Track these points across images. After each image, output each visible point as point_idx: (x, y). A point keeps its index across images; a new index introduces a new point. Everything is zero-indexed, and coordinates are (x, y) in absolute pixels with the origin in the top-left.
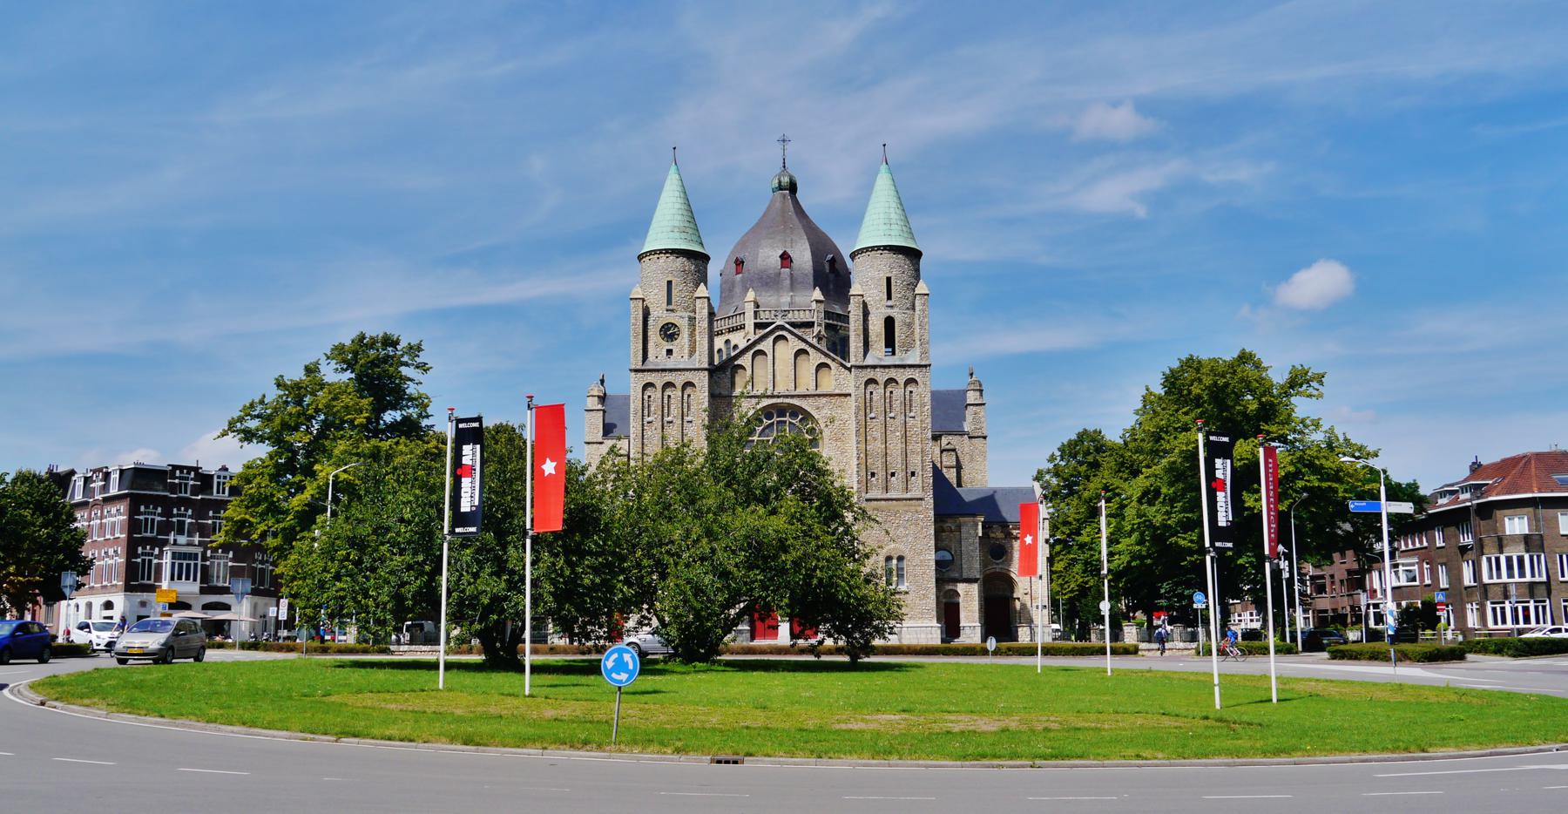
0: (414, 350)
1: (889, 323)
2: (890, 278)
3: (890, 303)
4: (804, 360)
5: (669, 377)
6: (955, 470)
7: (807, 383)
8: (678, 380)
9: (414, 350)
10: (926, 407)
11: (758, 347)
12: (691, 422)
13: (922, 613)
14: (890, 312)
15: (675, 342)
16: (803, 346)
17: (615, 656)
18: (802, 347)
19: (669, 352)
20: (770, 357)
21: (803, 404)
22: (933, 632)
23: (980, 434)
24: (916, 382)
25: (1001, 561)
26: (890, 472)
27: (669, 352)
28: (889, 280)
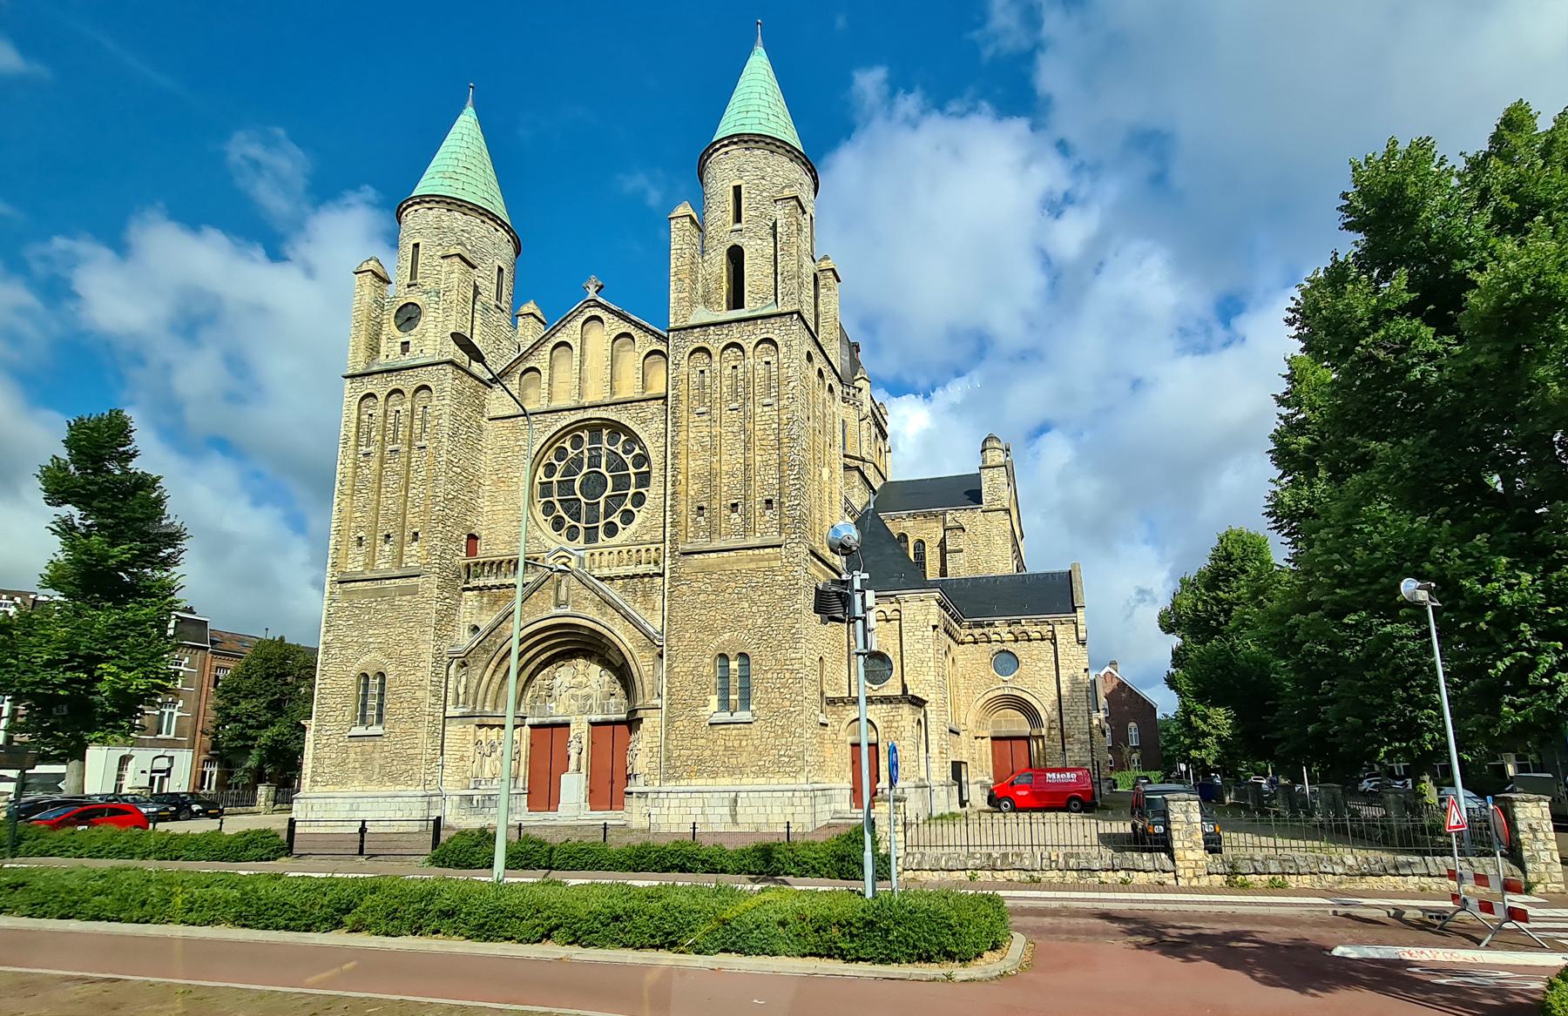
0: (130, 418)
2: (740, 186)
3: (738, 226)
4: (629, 350)
5: (610, 549)
6: (948, 548)
7: (629, 387)
9: (130, 418)
11: (560, 337)
12: (424, 447)
13: (778, 763)
14: (736, 240)
15: (414, 331)
16: (625, 327)
17: (23, 800)
18: (624, 330)
19: (405, 345)
20: (577, 351)
21: (624, 418)
22: (796, 801)
23: (999, 507)
24: (964, 531)
25: (1011, 677)
27: (405, 345)
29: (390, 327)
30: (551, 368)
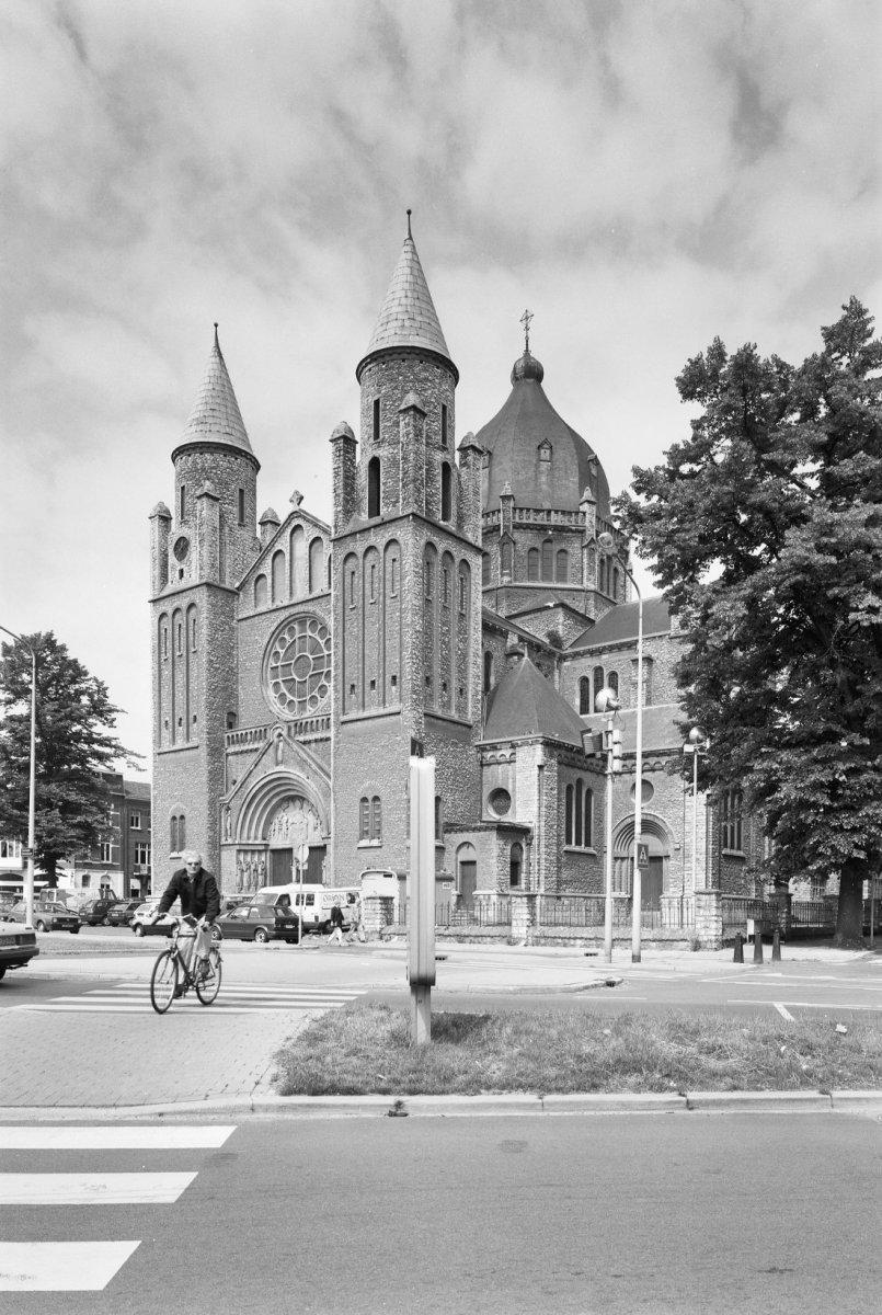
1: (375, 464)
8: (183, 602)
10: (408, 578)
26: (191, 717)
28: (377, 403)
29: (172, 559)
30: (273, 574)
